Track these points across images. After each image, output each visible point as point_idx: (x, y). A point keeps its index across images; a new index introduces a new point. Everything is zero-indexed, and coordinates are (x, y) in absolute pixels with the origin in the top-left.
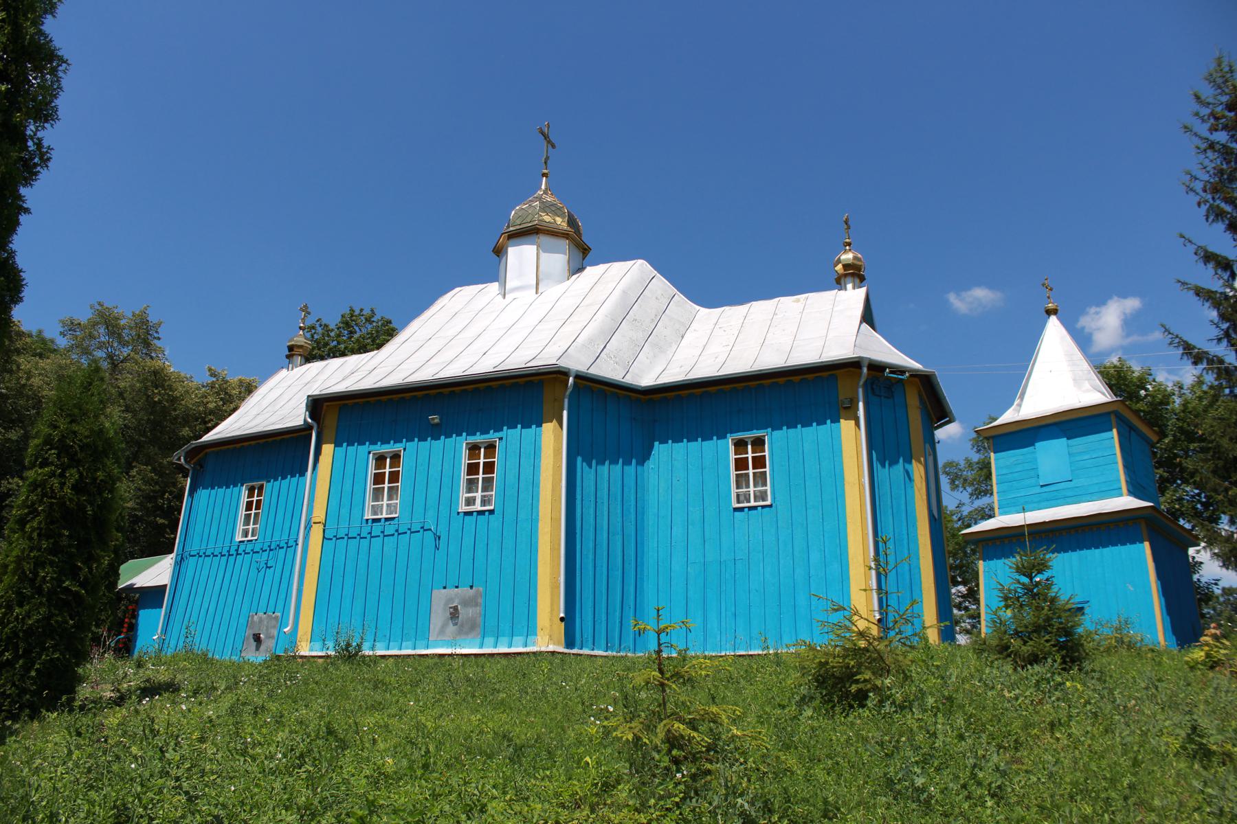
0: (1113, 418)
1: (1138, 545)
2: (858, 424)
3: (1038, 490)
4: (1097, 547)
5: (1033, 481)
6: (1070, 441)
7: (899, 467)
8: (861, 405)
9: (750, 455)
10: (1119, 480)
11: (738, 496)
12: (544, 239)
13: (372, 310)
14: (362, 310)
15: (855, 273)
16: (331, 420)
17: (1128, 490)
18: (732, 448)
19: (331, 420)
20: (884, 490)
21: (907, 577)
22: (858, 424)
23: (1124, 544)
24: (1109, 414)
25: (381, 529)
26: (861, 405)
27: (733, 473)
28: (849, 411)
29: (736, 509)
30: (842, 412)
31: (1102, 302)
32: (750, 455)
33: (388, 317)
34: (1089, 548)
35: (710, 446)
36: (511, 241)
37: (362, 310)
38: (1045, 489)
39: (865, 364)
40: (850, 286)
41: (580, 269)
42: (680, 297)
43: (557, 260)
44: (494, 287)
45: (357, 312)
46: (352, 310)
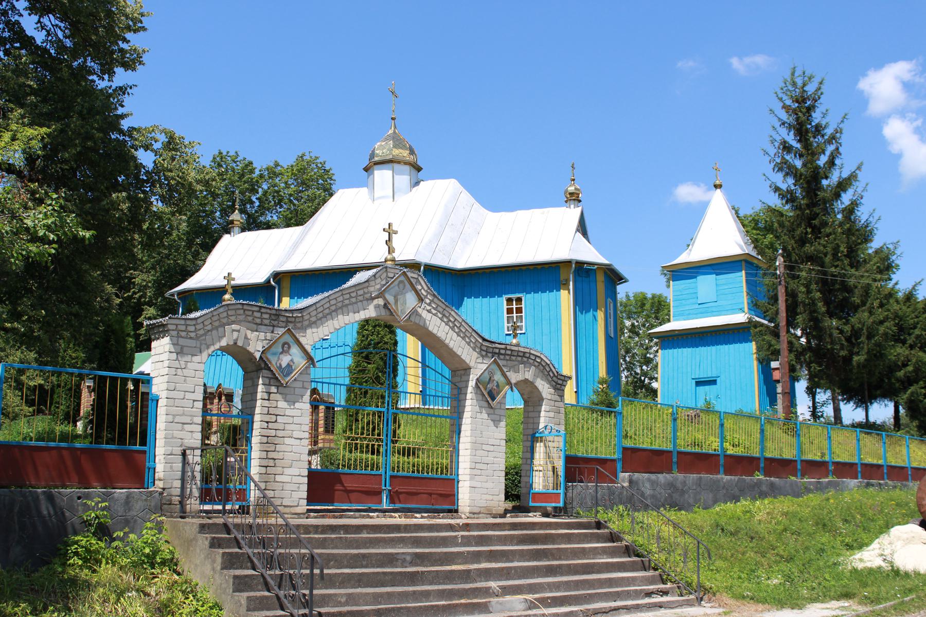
0: (743, 263)
1: (749, 344)
2: (569, 292)
3: (697, 306)
4: (726, 344)
5: (694, 300)
6: (718, 277)
7: (590, 315)
8: (571, 283)
9: (514, 306)
10: (743, 303)
11: (508, 327)
12: (396, 166)
13: (236, 153)
14: (228, 152)
15: (574, 198)
16: (286, 283)
17: (749, 309)
18: (505, 302)
19: (286, 283)
20: (581, 325)
21: (592, 370)
22: (569, 292)
23: (741, 343)
24: (741, 261)
25: (320, 345)
26: (571, 283)
27: (506, 315)
28: (565, 285)
29: (507, 335)
30: (562, 286)
31: (879, 64)
32: (514, 306)
33: (249, 159)
34: (722, 344)
35: (494, 301)
36: (376, 167)
37: (228, 152)
38: (701, 306)
39: (574, 262)
40: (572, 206)
41: (417, 183)
42: (477, 205)
43: (404, 179)
44: (364, 191)
45: (225, 153)
46: (220, 153)
